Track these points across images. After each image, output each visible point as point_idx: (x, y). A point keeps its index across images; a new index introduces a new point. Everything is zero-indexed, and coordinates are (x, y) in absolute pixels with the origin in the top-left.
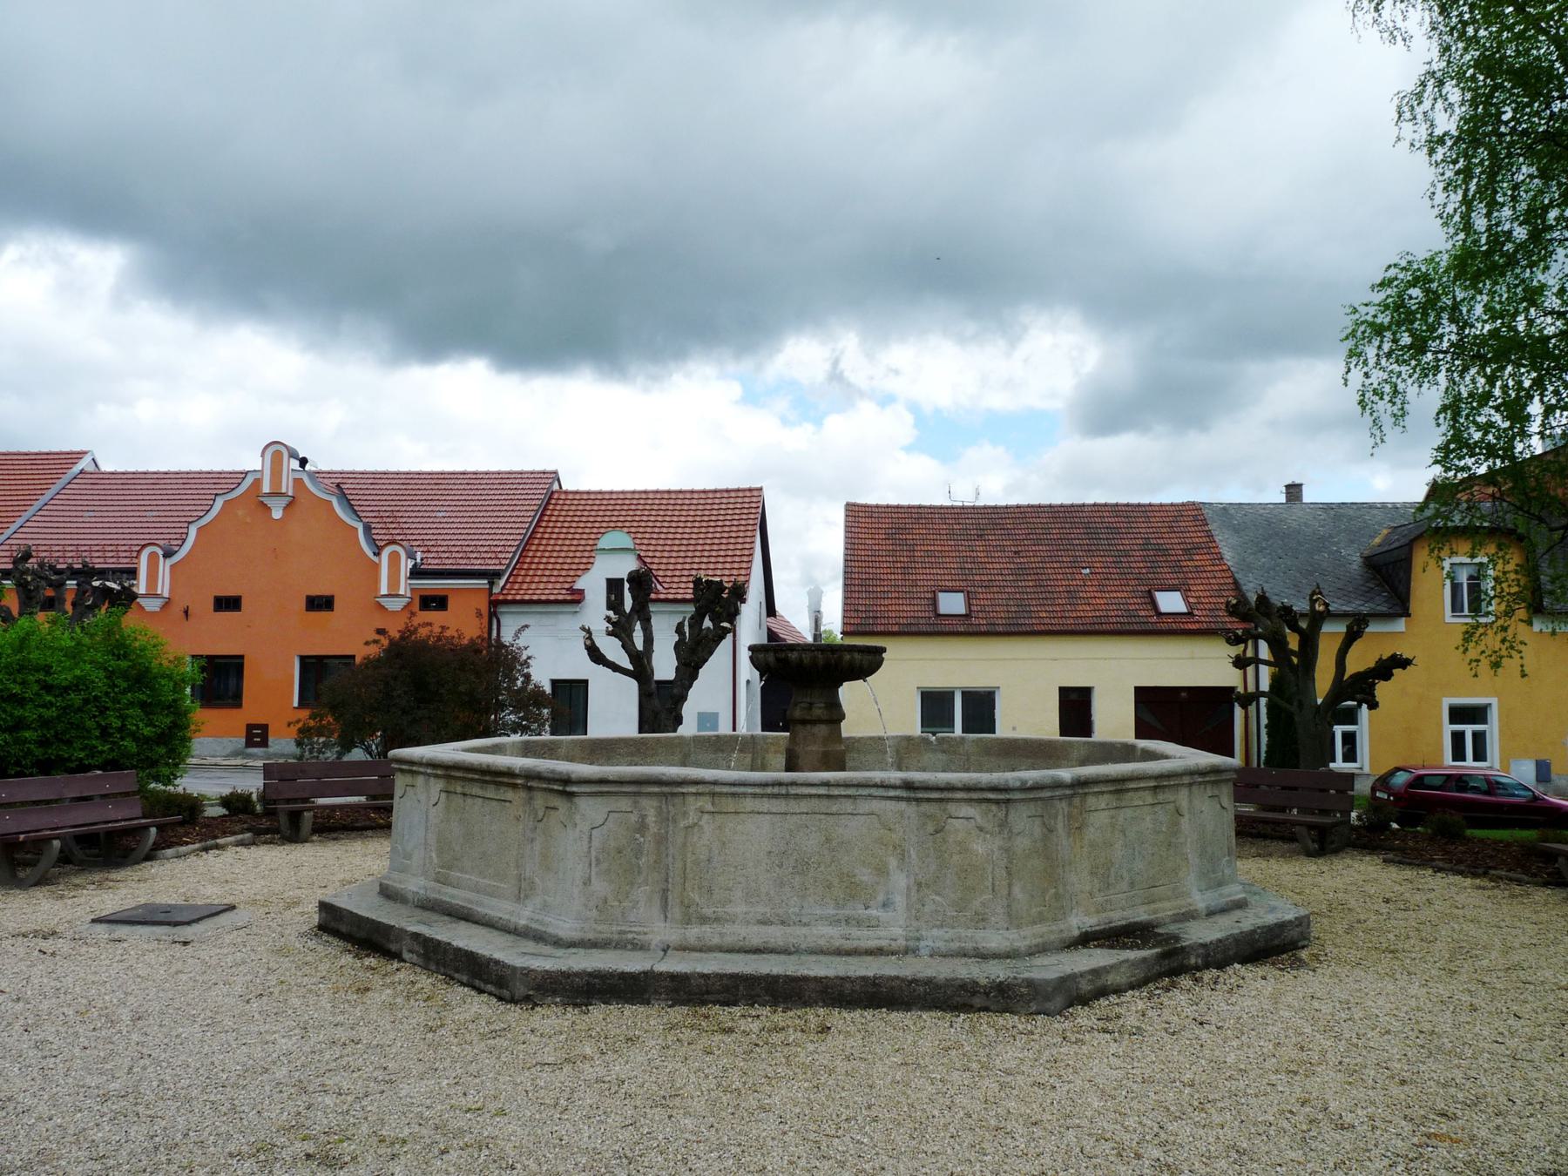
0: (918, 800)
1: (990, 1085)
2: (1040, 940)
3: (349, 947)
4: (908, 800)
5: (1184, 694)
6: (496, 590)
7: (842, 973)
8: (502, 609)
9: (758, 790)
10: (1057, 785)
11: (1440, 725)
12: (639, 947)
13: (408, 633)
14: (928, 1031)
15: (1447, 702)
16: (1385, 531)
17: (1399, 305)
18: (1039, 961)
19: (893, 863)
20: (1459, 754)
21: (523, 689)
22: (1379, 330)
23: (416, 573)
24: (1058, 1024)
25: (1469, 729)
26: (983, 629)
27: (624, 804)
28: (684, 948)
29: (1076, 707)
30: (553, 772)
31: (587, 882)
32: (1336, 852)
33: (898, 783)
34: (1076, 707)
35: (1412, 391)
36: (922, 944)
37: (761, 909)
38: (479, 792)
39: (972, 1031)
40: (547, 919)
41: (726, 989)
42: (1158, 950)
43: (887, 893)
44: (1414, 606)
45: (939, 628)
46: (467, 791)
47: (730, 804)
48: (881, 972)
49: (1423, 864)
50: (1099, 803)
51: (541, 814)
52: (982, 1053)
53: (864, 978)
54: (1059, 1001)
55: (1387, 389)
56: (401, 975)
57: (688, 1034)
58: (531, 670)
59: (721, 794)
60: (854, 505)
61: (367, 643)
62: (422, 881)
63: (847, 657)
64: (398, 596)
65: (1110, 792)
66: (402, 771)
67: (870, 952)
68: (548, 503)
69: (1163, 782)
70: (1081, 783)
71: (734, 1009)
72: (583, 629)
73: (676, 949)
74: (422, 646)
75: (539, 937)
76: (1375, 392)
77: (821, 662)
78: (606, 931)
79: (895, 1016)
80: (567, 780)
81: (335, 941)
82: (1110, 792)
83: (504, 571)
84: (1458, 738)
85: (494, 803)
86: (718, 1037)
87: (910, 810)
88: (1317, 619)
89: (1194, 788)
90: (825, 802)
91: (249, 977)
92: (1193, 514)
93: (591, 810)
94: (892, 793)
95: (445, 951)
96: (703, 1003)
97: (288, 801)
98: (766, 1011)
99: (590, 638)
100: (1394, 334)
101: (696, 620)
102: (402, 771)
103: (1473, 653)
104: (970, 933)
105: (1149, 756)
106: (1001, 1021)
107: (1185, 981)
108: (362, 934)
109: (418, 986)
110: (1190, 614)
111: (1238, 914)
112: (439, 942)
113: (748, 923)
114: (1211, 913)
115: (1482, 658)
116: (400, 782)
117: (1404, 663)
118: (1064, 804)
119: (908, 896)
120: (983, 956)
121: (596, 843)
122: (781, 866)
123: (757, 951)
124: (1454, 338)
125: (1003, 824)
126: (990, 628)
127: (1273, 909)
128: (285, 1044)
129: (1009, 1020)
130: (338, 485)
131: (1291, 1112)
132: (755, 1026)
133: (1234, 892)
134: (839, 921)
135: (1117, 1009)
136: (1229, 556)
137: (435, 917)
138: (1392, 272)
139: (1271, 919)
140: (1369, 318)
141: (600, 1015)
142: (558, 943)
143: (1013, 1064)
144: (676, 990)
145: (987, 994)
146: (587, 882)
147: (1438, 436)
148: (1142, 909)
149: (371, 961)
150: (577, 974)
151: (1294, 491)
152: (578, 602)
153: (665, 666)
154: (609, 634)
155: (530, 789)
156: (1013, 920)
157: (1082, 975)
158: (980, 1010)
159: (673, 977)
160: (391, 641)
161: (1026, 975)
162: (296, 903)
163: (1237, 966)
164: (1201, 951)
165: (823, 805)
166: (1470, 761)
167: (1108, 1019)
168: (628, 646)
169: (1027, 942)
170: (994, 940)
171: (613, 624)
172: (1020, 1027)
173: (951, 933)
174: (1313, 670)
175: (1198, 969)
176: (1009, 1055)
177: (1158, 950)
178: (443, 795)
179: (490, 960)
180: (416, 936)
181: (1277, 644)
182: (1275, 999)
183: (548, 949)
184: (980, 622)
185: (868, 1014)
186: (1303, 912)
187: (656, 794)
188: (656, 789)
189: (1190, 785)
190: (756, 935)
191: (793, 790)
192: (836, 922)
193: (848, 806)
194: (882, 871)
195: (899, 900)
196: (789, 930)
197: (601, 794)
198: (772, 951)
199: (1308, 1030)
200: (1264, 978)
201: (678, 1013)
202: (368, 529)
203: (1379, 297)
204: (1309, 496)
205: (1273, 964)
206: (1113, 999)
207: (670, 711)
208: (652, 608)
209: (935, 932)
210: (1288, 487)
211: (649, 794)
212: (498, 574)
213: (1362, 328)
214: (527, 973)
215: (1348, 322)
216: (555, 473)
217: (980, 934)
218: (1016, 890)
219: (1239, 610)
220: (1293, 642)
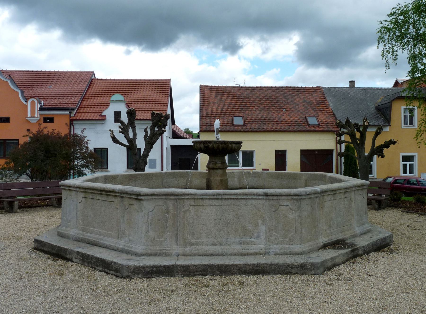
0: (269, 200)
1: (308, 303)
2: (311, 247)
3: (49, 256)
4: (266, 199)
5: (317, 152)
6: (72, 115)
7: (245, 263)
8: (74, 122)
9: (211, 197)
10: (316, 193)
11: (399, 162)
12: (167, 255)
13: (39, 132)
14: (279, 282)
15: (402, 154)
16: (382, 97)
17: (396, 22)
18: (312, 255)
19: (260, 222)
20: (405, 172)
21: (86, 152)
22: (389, 30)
23: (41, 109)
24: (323, 278)
25: (408, 163)
26: (250, 130)
27: (160, 203)
28: (185, 255)
29: (281, 157)
30: (132, 191)
31: (147, 232)
32: (384, 208)
33: (262, 194)
34: (281, 157)
35: (400, 51)
36: (271, 250)
37: (212, 240)
38: (100, 198)
39: (294, 282)
40: (131, 246)
41: (203, 270)
42: (350, 249)
43: (258, 232)
44: (392, 123)
45: (234, 130)
46: (94, 197)
47: (201, 202)
48: (259, 262)
49: (416, 212)
50: (328, 198)
51: (127, 207)
52: (301, 290)
53: (253, 264)
54: (322, 269)
55: (391, 50)
56: (74, 268)
57: (193, 288)
58: (88, 145)
59: (197, 199)
60: (203, 86)
61: (24, 136)
62: (75, 231)
63: (230, 145)
64: (35, 117)
65: (331, 195)
66: (65, 189)
67: (252, 254)
68: (91, 83)
69: (347, 190)
70: (323, 192)
71: (206, 277)
72: (110, 130)
73: (181, 255)
74: (47, 137)
75: (128, 252)
76: (387, 51)
77: (221, 148)
78: (155, 249)
79: (265, 277)
80: (138, 195)
81: (43, 254)
82: (331, 195)
83: (75, 108)
84: (405, 166)
85: (106, 202)
86: (205, 289)
87: (266, 203)
88: (366, 128)
89: (356, 192)
90: (235, 200)
91: (13, 271)
92: (319, 90)
93: (148, 205)
94: (260, 197)
95: (92, 258)
96: (195, 275)
97: (7, 198)
98: (218, 277)
99: (113, 134)
100: (394, 31)
101: (152, 128)
102: (65, 189)
103: (419, 140)
104: (288, 246)
105: (341, 181)
106: (303, 278)
107: (358, 259)
108: (55, 252)
109: (82, 272)
110: (319, 125)
111: (370, 234)
112: (89, 255)
113: (208, 245)
114: (361, 235)
115: (422, 141)
116: (65, 194)
117: (393, 142)
118: (317, 199)
119: (266, 233)
120: (293, 254)
121: (150, 218)
122: (219, 224)
123: (212, 255)
124: (414, 34)
125: (299, 207)
126: (251, 130)
127: (380, 232)
128: (39, 299)
129: (305, 277)
130: (9, 76)
131: (414, 308)
132: (216, 283)
133: (367, 227)
134: (241, 243)
135: (340, 271)
136: (331, 105)
137: (83, 245)
138: (394, 10)
139: (381, 236)
140: (386, 26)
141: (157, 281)
142: (136, 254)
143: (313, 294)
144: (185, 271)
145: (297, 268)
146: (147, 232)
147: (409, 68)
148: (341, 234)
149: (60, 262)
150: (147, 267)
151: (352, 83)
152: (104, 120)
153: (141, 144)
154: (120, 132)
155: (122, 197)
156: (303, 241)
157: (328, 260)
158: (294, 274)
159: (183, 266)
160: (33, 134)
161: (310, 261)
162: (21, 238)
163: (373, 253)
164: (362, 249)
165: (234, 202)
166: (408, 174)
167: (338, 275)
168: (127, 137)
169: (307, 249)
170: (296, 248)
171: (122, 129)
172: (310, 279)
173: (281, 246)
174: (364, 145)
175: (362, 255)
176: (310, 291)
177: (350, 249)
178: (84, 199)
179: (112, 262)
180: (78, 253)
181: (352, 136)
182: (390, 264)
183: (133, 257)
184: (248, 127)
185: (255, 277)
186: (391, 233)
187: (173, 199)
188: (173, 197)
189: (355, 191)
190: (211, 249)
191: (224, 197)
192: (239, 243)
193: (244, 202)
194: (256, 225)
195: (263, 236)
196: (223, 247)
197: (152, 199)
198: (217, 255)
199: (405, 276)
200: (383, 257)
201: (186, 280)
202: (22, 92)
203: (389, 19)
204: (357, 86)
205: (384, 251)
206: (338, 267)
207: (143, 160)
208: (136, 122)
209: (275, 246)
210: (350, 82)
211: (170, 199)
212: (73, 110)
213: (383, 29)
214: (128, 267)
215: (379, 27)
216: (93, 72)
217: (291, 246)
218: (303, 230)
219: (340, 125)
220: (358, 135)
